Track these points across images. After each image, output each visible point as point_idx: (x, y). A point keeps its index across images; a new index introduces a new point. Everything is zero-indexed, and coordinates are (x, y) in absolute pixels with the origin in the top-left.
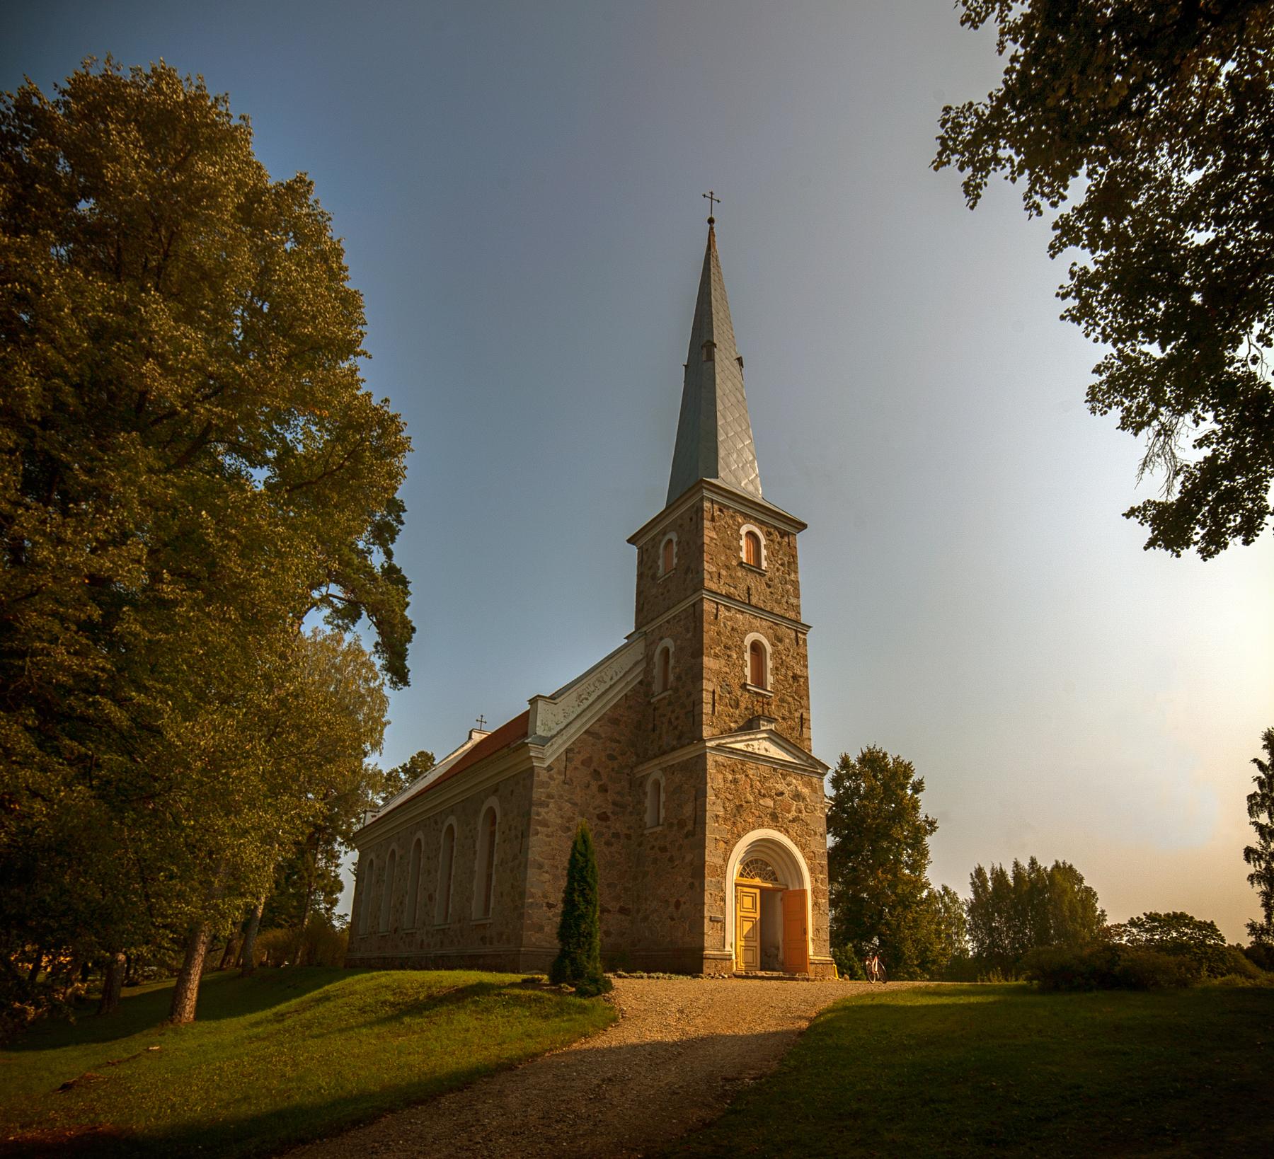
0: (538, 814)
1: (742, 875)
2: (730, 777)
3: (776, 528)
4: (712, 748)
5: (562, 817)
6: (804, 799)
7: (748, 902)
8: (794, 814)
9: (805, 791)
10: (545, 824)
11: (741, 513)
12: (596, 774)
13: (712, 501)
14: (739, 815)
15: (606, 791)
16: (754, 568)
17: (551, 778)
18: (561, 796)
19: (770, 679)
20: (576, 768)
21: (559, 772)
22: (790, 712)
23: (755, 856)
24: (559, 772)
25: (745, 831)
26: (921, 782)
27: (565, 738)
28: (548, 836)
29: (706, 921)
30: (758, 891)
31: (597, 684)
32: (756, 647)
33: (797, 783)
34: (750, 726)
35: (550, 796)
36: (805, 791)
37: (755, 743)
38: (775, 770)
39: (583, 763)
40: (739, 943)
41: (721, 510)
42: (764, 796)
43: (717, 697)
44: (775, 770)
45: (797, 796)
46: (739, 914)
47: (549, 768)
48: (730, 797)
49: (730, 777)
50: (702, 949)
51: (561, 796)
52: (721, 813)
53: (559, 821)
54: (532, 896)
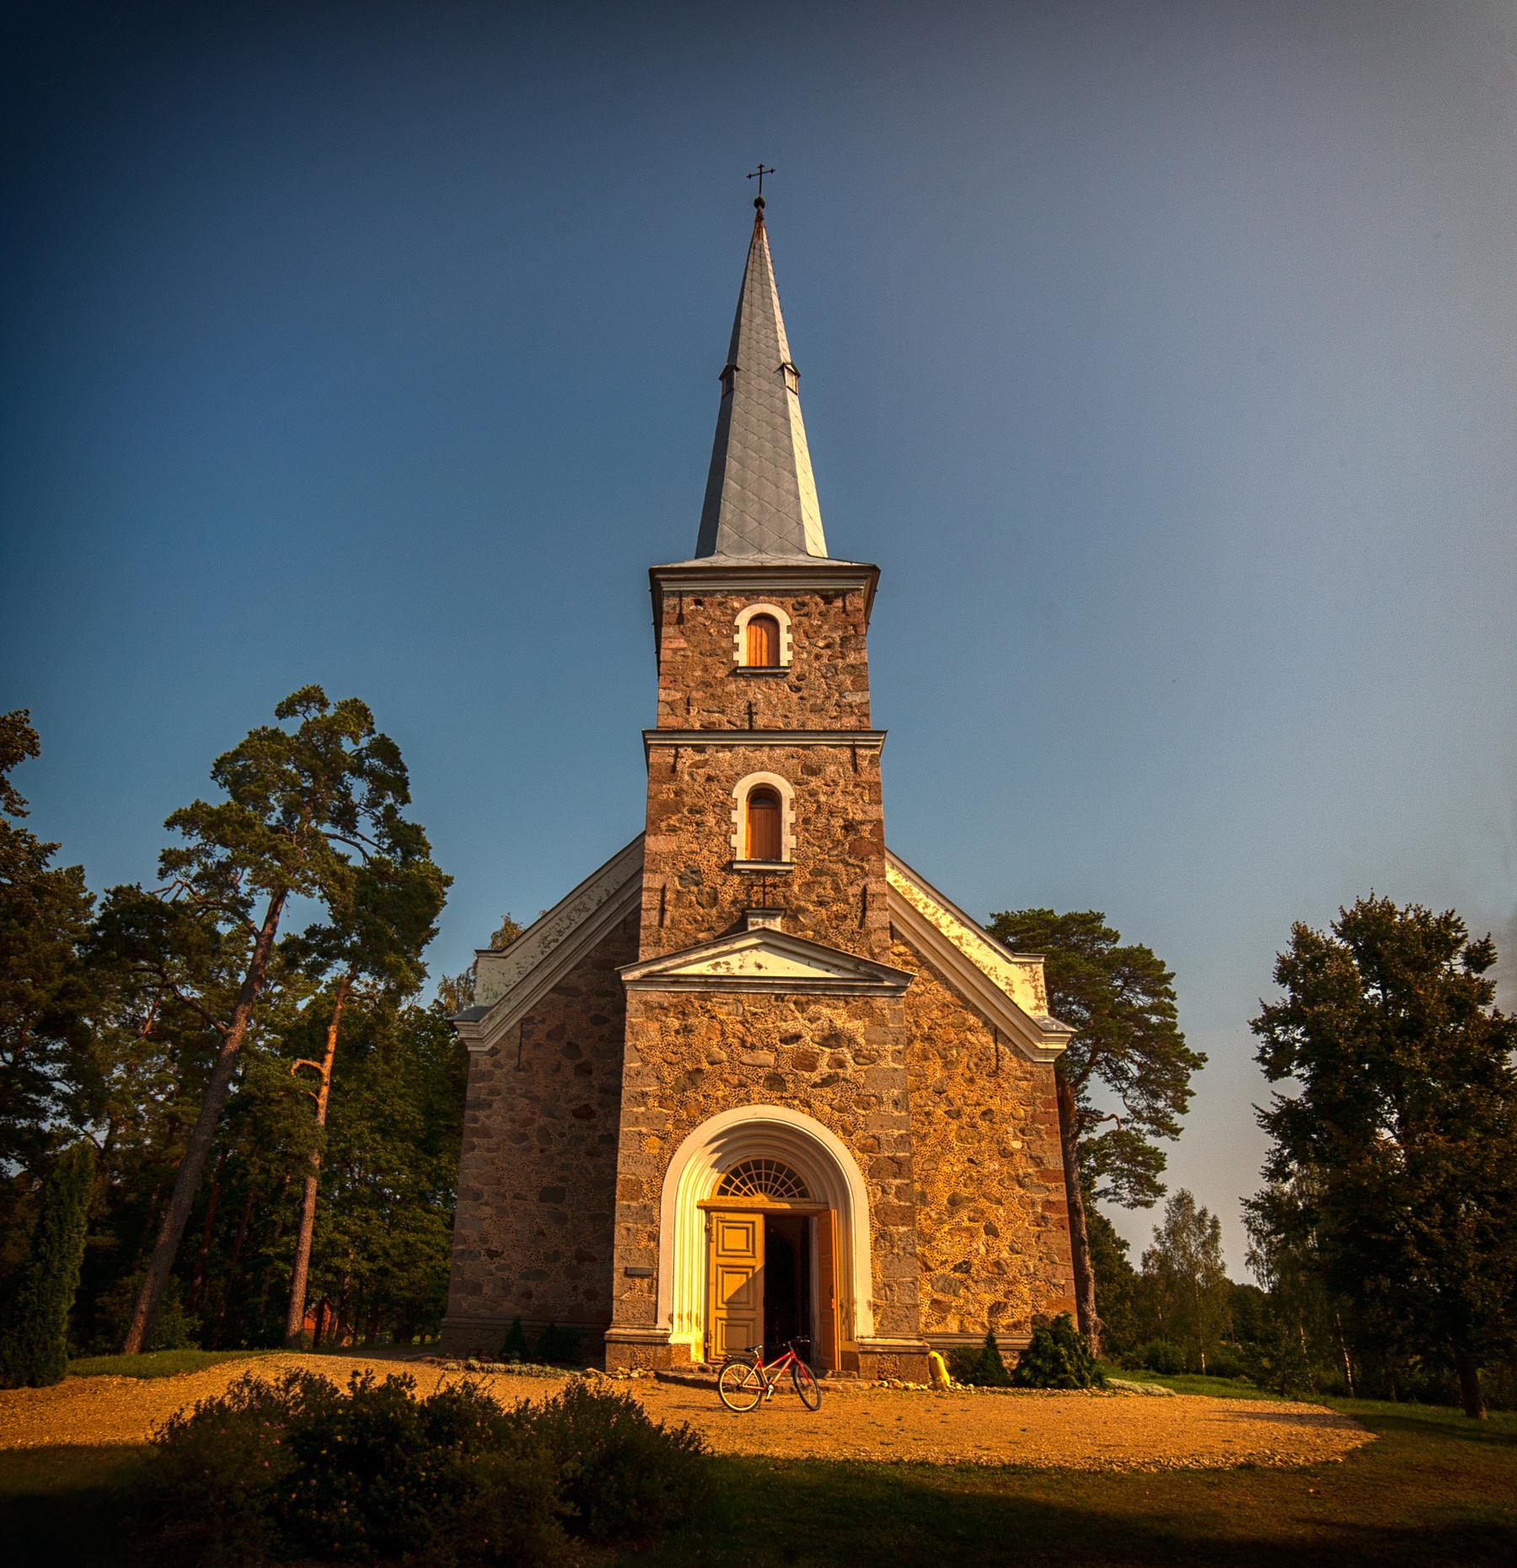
0: (475, 1120)
1: (722, 1191)
2: (676, 1024)
3: (807, 592)
4: (634, 982)
5: (512, 1120)
6: (851, 1040)
7: (735, 1240)
8: (824, 1068)
9: (856, 1027)
10: (485, 1133)
11: (739, 593)
12: (572, 1049)
13: (681, 594)
14: (690, 1092)
15: (590, 1072)
16: (769, 670)
17: (497, 1065)
18: (512, 1090)
19: (789, 841)
20: (538, 1045)
21: (510, 1055)
22: (837, 889)
23: (736, 1161)
24: (510, 1055)
25: (706, 1113)
26: (1486, 947)
27: (514, 1003)
28: (489, 1150)
29: (617, 1277)
30: (759, 1220)
31: (574, 915)
32: (764, 798)
33: (838, 1017)
34: (738, 928)
35: (493, 1092)
36: (856, 1027)
37: (734, 960)
38: (779, 997)
39: (549, 1036)
40: (713, 1314)
41: (698, 602)
42: (753, 1047)
43: (669, 896)
44: (779, 997)
45: (833, 1038)
46: (714, 1260)
47: (494, 1051)
48: (675, 1059)
49: (676, 1024)
50: (607, 1322)
51: (512, 1090)
52: (653, 1089)
53: (508, 1127)
54: (464, 1240)
